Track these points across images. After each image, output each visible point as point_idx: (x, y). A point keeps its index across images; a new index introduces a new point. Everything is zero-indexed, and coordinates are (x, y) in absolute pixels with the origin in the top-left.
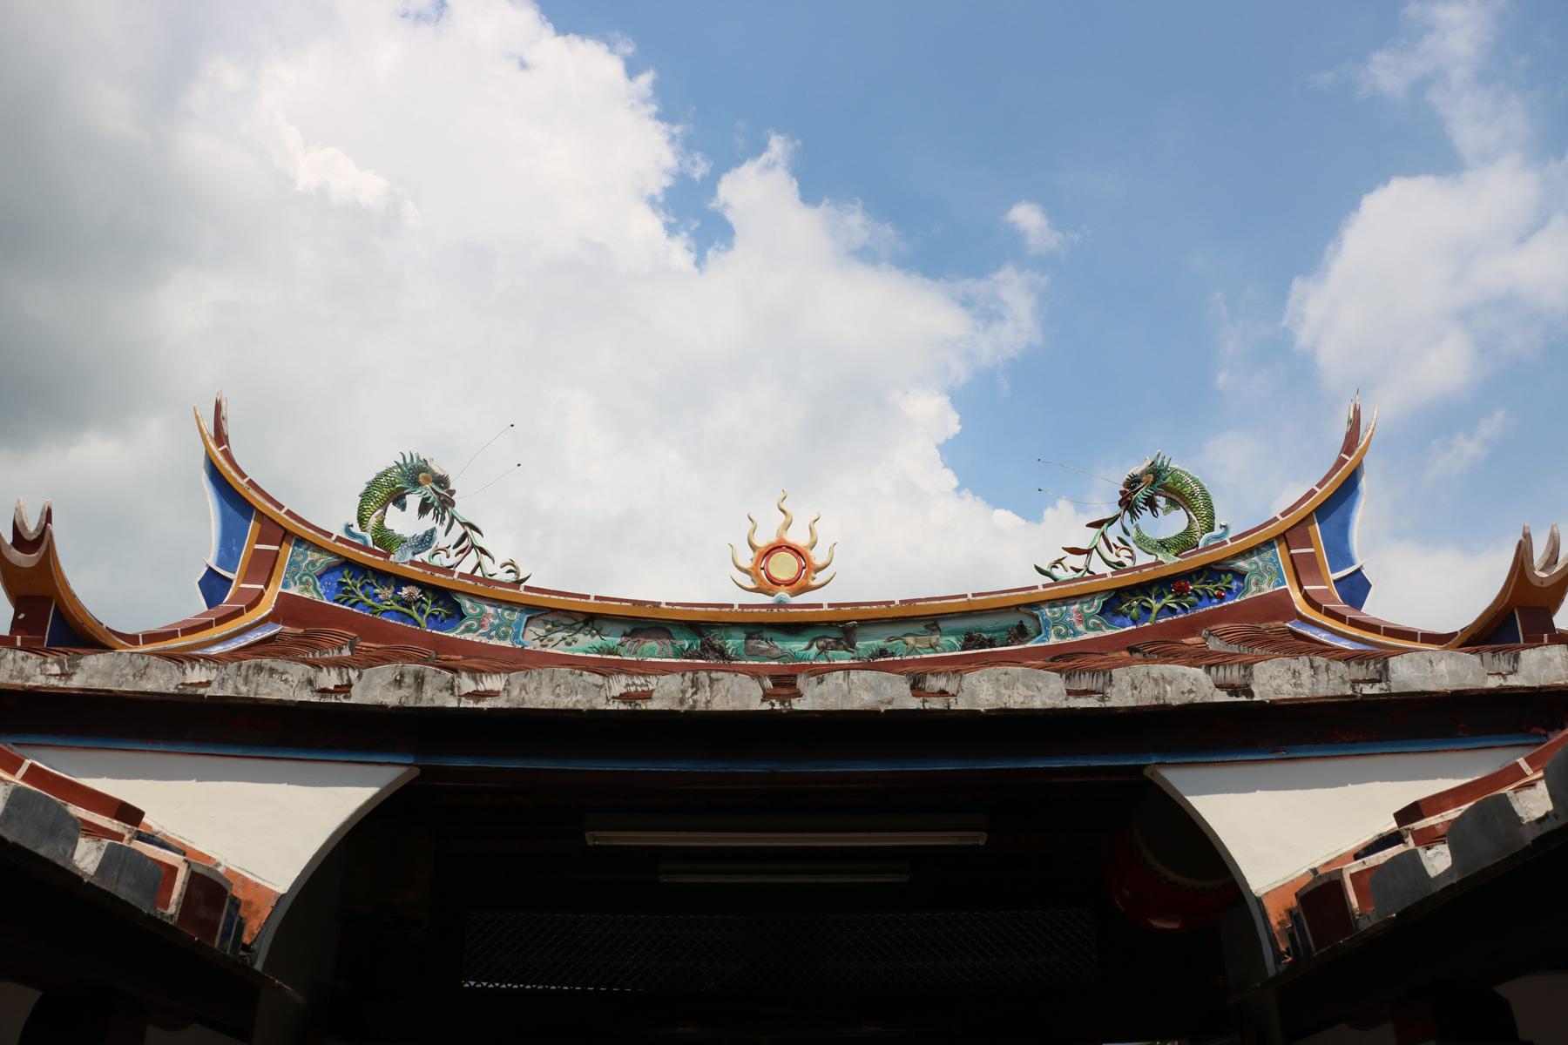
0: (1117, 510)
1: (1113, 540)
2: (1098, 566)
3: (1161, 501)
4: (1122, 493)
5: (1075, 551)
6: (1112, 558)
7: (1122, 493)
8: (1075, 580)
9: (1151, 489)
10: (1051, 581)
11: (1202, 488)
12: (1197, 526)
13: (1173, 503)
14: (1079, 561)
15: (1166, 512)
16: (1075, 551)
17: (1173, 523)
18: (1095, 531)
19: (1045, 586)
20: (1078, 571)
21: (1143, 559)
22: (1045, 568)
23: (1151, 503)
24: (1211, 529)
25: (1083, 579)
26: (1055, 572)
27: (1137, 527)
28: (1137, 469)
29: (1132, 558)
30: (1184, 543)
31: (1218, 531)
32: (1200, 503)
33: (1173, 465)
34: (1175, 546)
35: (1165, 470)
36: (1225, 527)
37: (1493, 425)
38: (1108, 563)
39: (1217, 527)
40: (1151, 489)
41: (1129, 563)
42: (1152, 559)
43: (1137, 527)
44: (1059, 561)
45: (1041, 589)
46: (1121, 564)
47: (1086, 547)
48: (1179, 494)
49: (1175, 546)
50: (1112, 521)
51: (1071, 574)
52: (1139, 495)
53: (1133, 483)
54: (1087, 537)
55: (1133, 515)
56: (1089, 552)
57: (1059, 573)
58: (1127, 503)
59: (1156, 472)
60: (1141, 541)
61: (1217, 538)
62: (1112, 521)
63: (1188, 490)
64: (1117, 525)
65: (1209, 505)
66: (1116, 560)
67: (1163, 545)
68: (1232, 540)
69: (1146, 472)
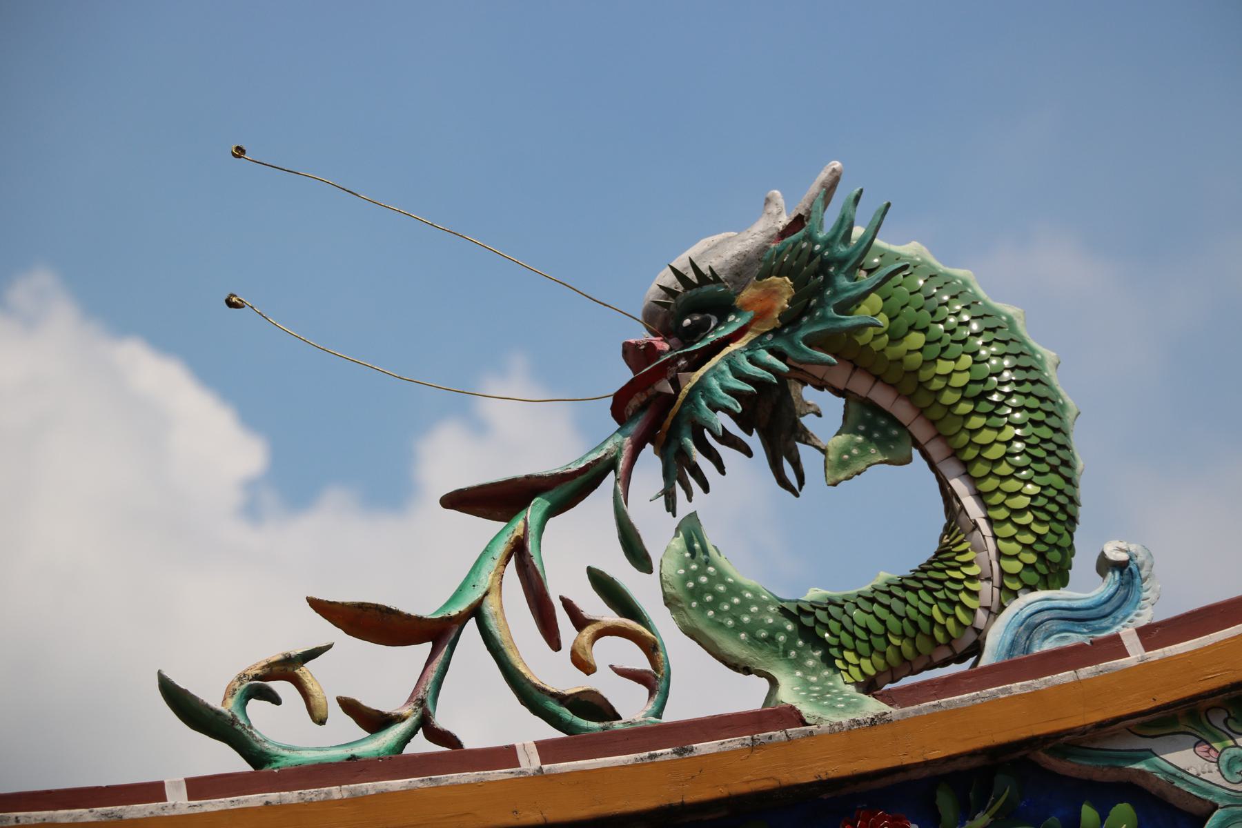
0: (606, 435)
1: (565, 581)
2: (480, 710)
3: (823, 413)
4: (634, 354)
5: (374, 623)
6: (555, 673)
7: (634, 354)
8: (353, 768)
9: (777, 346)
10: (239, 765)
11: (1029, 373)
12: (984, 551)
13: (877, 430)
14: (387, 676)
15: (842, 468)
16: (374, 623)
17: (827, 526)
18: (482, 531)
19: (199, 787)
20: (374, 722)
21: (705, 687)
22: (213, 692)
23: (772, 420)
24: (1054, 572)
25: (394, 763)
26: (259, 714)
27: (691, 531)
28: (719, 249)
29: (654, 680)
30: (911, 631)
31: (1085, 588)
32: (1008, 435)
33: (901, 244)
34: (869, 642)
35: (856, 262)
36: (1125, 572)
37: (749, 388)
38: (531, 696)
39: (1082, 564)
40: (777, 346)
41: (633, 705)
42: (746, 694)
43: (691, 531)
44: (287, 668)
45: (178, 801)
46: (593, 706)
47: (424, 602)
48: (911, 384)
49: (869, 642)
50: (568, 489)
51: (340, 738)
52: (717, 375)
53: (692, 309)
54: (435, 559)
55: (679, 471)
56: (439, 633)
57: (280, 725)
58: (656, 412)
59: (809, 266)
60: (706, 600)
61: (1076, 617)
62: (568, 489)
63: (955, 370)
64: (597, 507)
65: (1053, 456)
66: (567, 681)
67: (810, 630)
68: (1151, 635)
69: (760, 265)
